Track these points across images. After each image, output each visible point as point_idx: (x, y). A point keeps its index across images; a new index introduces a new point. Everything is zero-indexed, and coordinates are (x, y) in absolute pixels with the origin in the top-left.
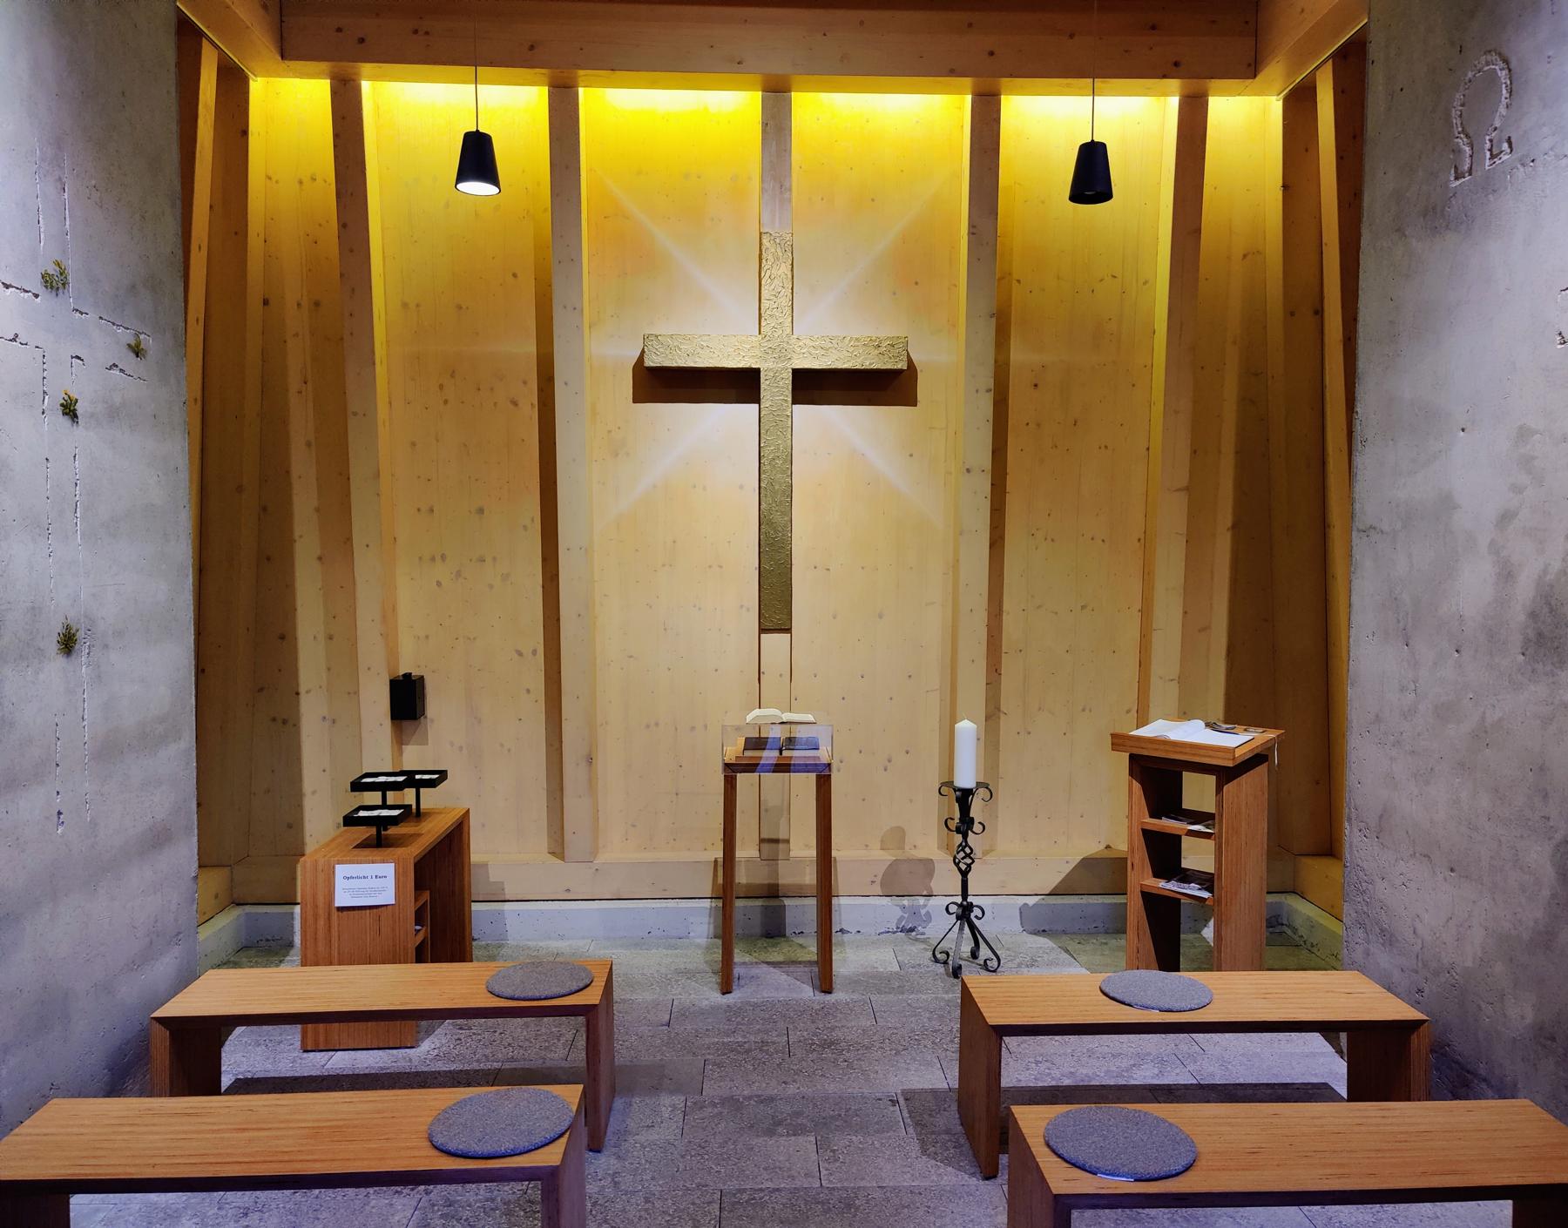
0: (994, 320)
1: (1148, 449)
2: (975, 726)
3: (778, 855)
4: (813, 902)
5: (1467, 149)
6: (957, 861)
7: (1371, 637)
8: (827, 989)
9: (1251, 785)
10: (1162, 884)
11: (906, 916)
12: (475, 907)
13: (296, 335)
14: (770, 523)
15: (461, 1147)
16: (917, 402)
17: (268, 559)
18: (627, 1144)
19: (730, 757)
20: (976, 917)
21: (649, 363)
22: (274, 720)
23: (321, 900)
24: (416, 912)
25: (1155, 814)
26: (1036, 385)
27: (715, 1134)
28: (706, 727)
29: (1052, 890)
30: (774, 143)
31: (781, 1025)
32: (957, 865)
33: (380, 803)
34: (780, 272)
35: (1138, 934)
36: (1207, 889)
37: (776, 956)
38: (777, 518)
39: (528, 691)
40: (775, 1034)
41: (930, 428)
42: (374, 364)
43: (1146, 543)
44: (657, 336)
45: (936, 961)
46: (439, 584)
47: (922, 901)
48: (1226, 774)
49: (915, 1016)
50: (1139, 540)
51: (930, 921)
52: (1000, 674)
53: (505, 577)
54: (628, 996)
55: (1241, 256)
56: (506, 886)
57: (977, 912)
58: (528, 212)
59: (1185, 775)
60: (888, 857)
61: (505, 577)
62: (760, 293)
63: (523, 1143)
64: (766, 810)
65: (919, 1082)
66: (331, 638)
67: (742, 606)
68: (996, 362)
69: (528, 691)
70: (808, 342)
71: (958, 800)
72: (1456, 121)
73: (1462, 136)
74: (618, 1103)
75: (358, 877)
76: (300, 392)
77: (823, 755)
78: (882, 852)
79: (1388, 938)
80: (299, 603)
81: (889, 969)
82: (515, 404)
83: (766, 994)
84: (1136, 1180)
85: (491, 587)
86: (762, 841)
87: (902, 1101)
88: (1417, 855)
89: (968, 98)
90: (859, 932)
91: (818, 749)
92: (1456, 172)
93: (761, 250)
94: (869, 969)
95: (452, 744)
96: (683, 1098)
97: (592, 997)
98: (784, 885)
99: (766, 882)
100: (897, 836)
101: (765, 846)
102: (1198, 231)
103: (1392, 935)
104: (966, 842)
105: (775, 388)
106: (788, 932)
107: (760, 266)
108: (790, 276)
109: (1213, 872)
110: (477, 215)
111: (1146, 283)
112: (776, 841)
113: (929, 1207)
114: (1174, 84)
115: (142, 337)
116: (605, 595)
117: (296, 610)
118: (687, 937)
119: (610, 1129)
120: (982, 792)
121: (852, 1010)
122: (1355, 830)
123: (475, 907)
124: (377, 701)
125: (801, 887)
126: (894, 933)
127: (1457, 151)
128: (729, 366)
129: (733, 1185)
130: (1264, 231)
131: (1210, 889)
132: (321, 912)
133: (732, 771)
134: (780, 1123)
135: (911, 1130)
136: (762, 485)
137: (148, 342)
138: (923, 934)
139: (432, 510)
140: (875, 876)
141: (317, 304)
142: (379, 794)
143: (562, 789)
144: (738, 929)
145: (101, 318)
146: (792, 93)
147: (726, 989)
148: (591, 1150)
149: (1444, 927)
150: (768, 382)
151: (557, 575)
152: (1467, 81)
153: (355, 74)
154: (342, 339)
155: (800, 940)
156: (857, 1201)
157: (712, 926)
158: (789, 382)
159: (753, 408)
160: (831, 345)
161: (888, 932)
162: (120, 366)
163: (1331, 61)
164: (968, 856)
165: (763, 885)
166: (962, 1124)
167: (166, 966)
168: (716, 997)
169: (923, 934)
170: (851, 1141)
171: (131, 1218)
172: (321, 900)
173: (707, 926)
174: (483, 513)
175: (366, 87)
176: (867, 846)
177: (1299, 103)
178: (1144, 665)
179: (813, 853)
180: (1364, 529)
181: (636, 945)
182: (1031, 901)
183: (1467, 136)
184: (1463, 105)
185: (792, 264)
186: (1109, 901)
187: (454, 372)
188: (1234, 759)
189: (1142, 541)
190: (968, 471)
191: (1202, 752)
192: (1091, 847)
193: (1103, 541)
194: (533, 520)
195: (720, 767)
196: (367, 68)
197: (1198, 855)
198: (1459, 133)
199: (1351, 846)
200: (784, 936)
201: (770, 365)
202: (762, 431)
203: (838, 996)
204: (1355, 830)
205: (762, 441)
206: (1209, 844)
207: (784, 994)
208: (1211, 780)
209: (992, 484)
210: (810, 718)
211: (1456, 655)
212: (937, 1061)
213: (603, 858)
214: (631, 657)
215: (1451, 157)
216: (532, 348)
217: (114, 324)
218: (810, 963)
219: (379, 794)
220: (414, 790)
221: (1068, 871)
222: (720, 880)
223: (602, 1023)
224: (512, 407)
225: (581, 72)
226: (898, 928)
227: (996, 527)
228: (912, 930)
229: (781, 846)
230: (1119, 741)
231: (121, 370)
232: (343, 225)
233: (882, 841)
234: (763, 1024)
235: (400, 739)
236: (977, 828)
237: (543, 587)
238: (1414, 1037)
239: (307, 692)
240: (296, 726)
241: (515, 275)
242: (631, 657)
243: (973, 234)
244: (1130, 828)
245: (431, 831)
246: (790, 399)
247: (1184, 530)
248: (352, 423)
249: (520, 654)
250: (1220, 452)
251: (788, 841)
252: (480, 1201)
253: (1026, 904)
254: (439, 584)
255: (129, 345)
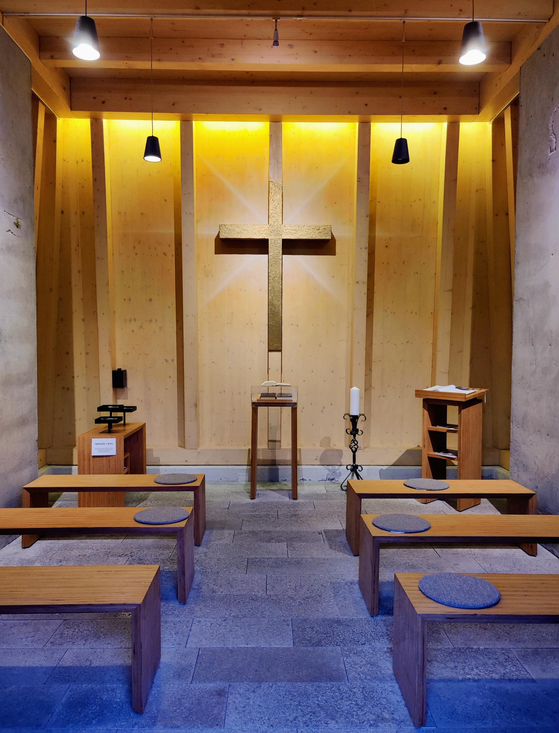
0: (368, 218)
1: (435, 274)
2: (359, 389)
3: (276, 447)
4: (290, 467)
5: (554, 140)
6: (351, 447)
7: (520, 344)
8: (295, 498)
9: (474, 411)
10: (436, 453)
11: (330, 473)
12: (148, 467)
13: (75, 226)
14: (273, 305)
15: (146, 521)
16: (335, 253)
17: (62, 320)
18: (210, 544)
19: (255, 400)
20: (359, 470)
21: (221, 237)
22: (63, 388)
23: (86, 453)
24: (124, 459)
25: (433, 424)
26: (387, 246)
27: (246, 542)
28: (245, 393)
29: (395, 462)
30: (275, 143)
31: (275, 509)
32: (351, 448)
33: (109, 416)
34: (277, 198)
35: (427, 475)
36: (455, 455)
37: (274, 488)
38: (276, 302)
39: (170, 377)
40: (272, 512)
41: (341, 265)
42: (107, 237)
43: (434, 314)
44: (225, 225)
45: (343, 490)
46: (133, 331)
47: (337, 467)
48: (464, 405)
49: (331, 507)
50: (432, 313)
51: (341, 476)
52: (371, 371)
53: (161, 328)
54: (212, 500)
55: (475, 191)
56: (160, 459)
57: (359, 468)
58: (171, 173)
59: (448, 407)
60: (323, 449)
61: (161, 328)
62: (269, 207)
63: (170, 520)
64: (271, 428)
65: (330, 527)
66: (87, 354)
67: (261, 341)
68: (369, 236)
69: (170, 377)
70: (289, 227)
71: (351, 420)
72: (551, 128)
73: (553, 134)
74: (207, 532)
75: (101, 444)
76: (76, 250)
77: (294, 400)
78: (321, 447)
79: (526, 468)
80: (74, 340)
81: (322, 492)
82: (165, 254)
83: (270, 500)
84: (405, 533)
85: (155, 332)
86: (269, 441)
87: (323, 533)
88: (536, 431)
89: (357, 124)
90: (310, 480)
91: (291, 397)
92: (550, 150)
93: (269, 189)
94: (313, 492)
95: (138, 399)
96: (234, 531)
97: (197, 484)
98: (278, 460)
99: (270, 459)
100: (327, 440)
101: (270, 443)
102: (456, 180)
103: (527, 466)
104: (355, 439)
105: (275, 247)
106: (280, 479)
107: (269, 195)
108: (281, 200)
109: (457, 450)
110: (150, 175)
111: (434, 202)
112: (275, 441)
113: (331, 564)
114: (445, 117)
115: (19, 220)
116: (203, 336)
117: (73, 342)
118: (237, 481)
119: (203, 540)
120: (361, 418)
121: (305, 505)
122: (515, 426)
123: (148, 467)
124: (107, 380)
125: (285, 461)
126: (325, 480)
127: (550, 141)
128: (255, 238)
129: (252, 557)
130: (485, 179)
131: (456, 455)
132: (86, 457)
133: (255, 406)
134: (273, 539)
135: (326, 542)
136: (269, 288)
137: (21, 222)
138: (338, 481)
139: (130, 300)
140: (317, 457)
141: (83, 213)
142: (109, 413)
143: (184, 419)
144: (258, 478)
145: (4, 211)
146: (283, 123)
147: (253, 497)
148: (196, 545)
149: (545, 459)
150: (272, 245)
151: (183, 328)
152: (554, 112)
153: (100, 116)
154: (93, 227)
155: (285, 483)
156: (302, 562)
157: (247, 477)
158: (281, 244)
159: (265, 256)
160: (298, 229)
161: (323, 480)
162: (11, 231)
163: (510, 107)
164: (356, 445)
165: (269, 460)
166: (347, 540)
167: (26, 473)
168: (249, 500)
169: (338, 481)
170: (301, 545)
171: (15, 563)
172: (86, 453)
173: (245, 476)
174: (152, 301)
175: (105, 122)
176: (314, 445)
177: (498, 124)
178: (434, 367)
179: (290, 447)
180: (518, 299)
181: (215, 484)
182: (384, 468)
183: (555, 134)
184: (553, 122)
185: (282, 194)
186: (418, 468)
187: (140, 241)
188: (465, 398)
189: (433, 313)
190: (357, 282)
191: (453, 396)
192: (412, 446)
193: (416, 313)
194: (172, 304)
195: (250, 404)
196: (105, 114)
197: (452, 442)
198: (552, 133)
199: (513, 433)
200: (278, 481)
201: (273, 237)
202: (269, 265)
203: (299, 500)
204: (515, 426)
205: (269, 270)
206: (456, 435)
207: (277, 500)
208: (457, 408)
209: (368, 289)
210: (289, 384)
211: (550, 347)
212: (339, 521)
213: (200, 449)
214: (213, 362)
215: (549, 143)
216: (173, 231)
217: (9, 214)
218: (289, 490)
219: (109, 413)
220: (123, 413)
221: (400, 455)
222: (251, 458)
223: (200, 495)
224: (164, 256)
225: (194, 114)
226: (327, 478)
227: (370, 307)
228: (333, 479)
229: (277, 443)
230: (418, 393)
231: (12, 233)
232: (95, 180)
233: (321, 443)
234: (268, 509)
235: (116, 396)
236: (360, 433)
237: (177, 332)
238: (530, 501)
239: (78, 377)
240: (73, 391)
241: (165, 200)
242: (213, 362)
243: (359, 181)
244: (423, 430)
245: (129, 430)
246: (281, 252)
247: (450, 308)
248: (98, 262)
249: (167, 361)
250: (466, 275)
251: (280, 441)
252: (152, 559)
253: (382, 469)
254: (133, 331)
255: (15, 223)
